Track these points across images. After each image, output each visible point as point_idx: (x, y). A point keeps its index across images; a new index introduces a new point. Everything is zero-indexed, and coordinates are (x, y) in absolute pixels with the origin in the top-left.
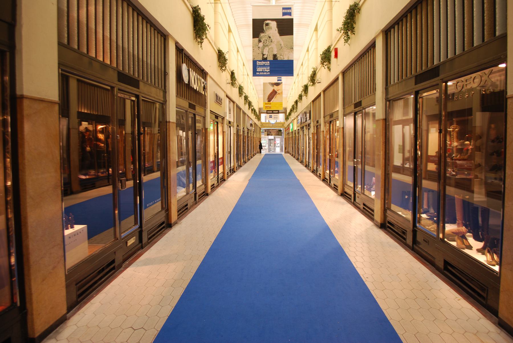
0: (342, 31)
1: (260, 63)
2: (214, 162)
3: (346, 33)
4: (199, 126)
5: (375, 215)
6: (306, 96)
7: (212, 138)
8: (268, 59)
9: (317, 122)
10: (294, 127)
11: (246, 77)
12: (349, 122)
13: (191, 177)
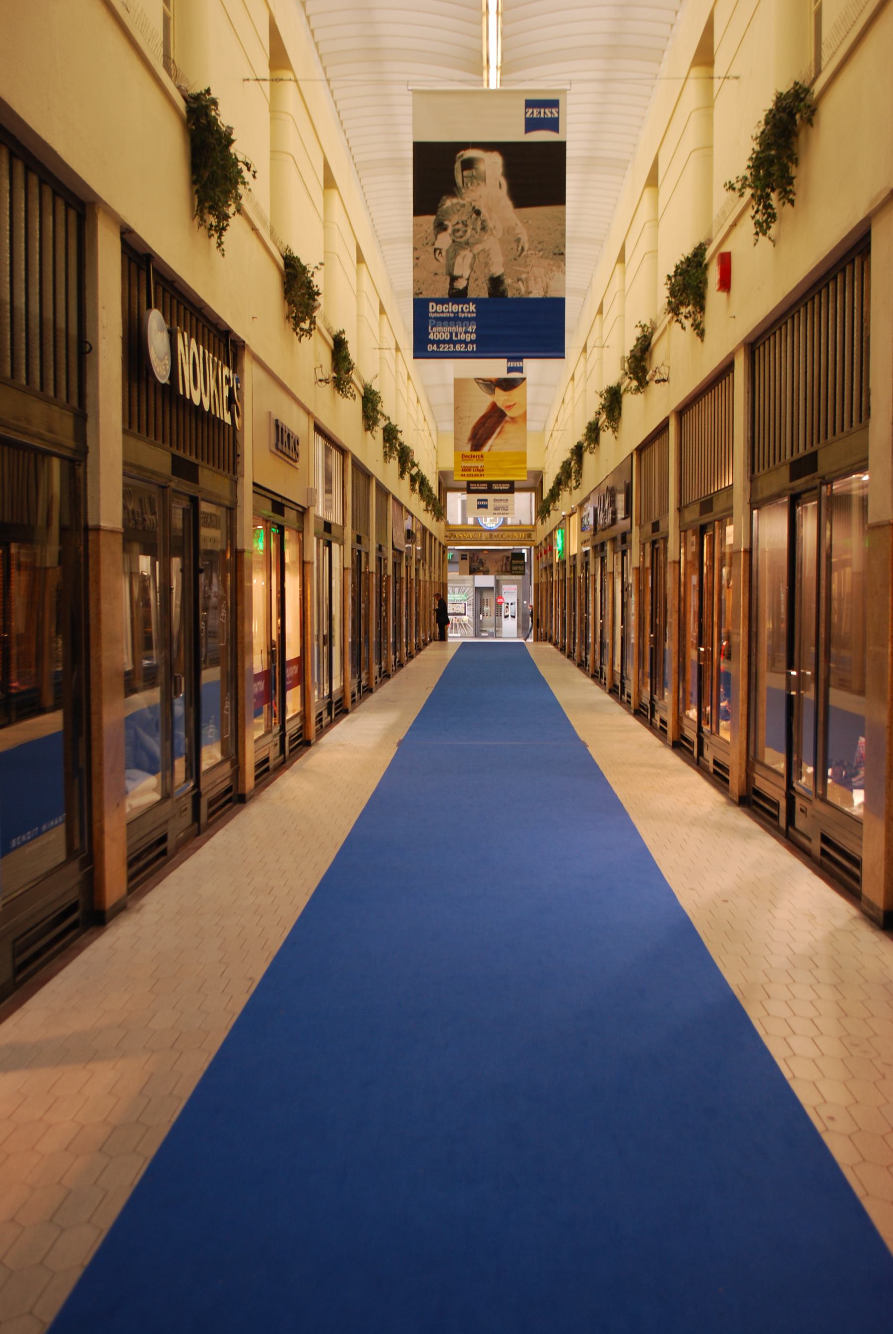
0: (748, 192)
1: (439, 308)
2: (266, 675)
3: (762, 199)
4: (211, 536)
5: (864, 880)
6: (615, 430)
7: (258, 584)
8: (471, 294)
9: (656, 527)
10: (571, 542)
11: (389, 355)
12: (772, 529)
13: (180, 733)
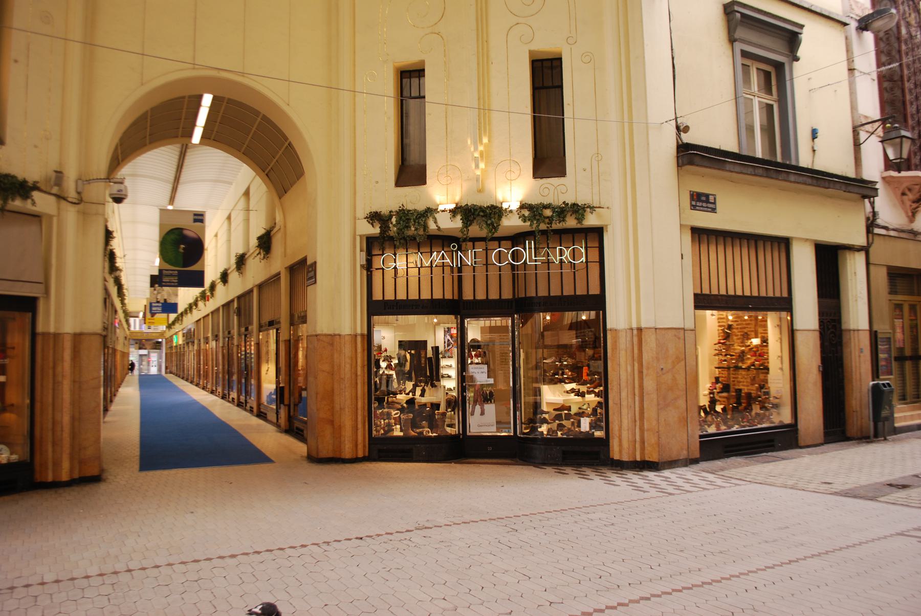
9: (229, 333)
10: (178, 340)
